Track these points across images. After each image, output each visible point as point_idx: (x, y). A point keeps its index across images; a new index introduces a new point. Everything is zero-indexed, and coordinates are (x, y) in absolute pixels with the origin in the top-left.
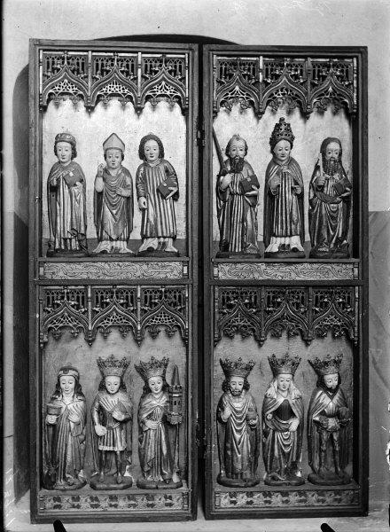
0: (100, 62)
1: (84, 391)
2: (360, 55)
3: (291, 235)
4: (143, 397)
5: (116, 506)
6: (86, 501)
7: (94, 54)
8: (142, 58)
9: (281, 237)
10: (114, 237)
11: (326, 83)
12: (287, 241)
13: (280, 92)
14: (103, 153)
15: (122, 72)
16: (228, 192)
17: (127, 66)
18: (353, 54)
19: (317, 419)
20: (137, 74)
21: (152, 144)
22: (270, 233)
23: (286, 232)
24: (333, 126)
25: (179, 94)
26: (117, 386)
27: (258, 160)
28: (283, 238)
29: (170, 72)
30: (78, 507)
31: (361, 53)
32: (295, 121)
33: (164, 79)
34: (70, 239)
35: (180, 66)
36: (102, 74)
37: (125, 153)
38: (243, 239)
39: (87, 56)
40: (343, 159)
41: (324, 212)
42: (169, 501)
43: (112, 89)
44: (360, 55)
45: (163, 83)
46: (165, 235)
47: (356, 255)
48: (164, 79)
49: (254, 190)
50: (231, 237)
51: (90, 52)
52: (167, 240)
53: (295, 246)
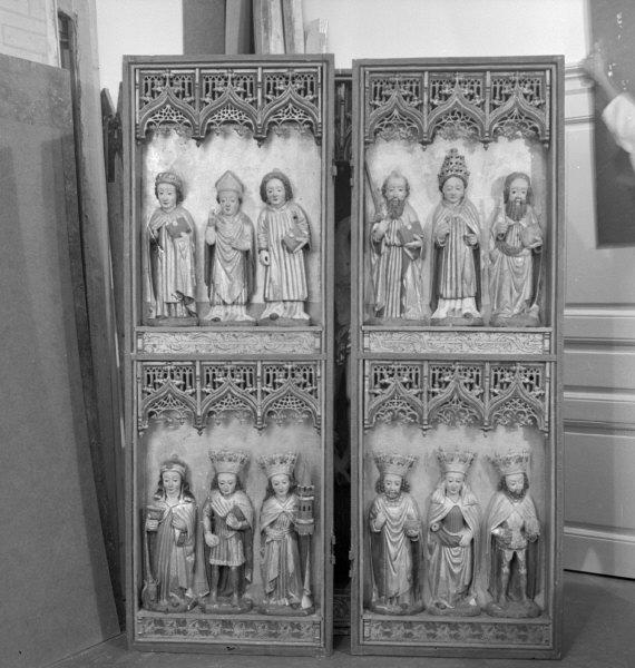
1: (194, 490)
4: (266, 499)
5: (230, 634)
6: (172, 625)
7: (496, 74)
8: (492, 77)
10: (229, 301)
11: (510, 103)
12: (457, 304)
13: (450, 117)
15: (239, 94)
19: (497, 532)
20: (422, 99)
21: (275, 184)
22: (436, 297)
25: (310, 119)
26: (234, 485)
27: (422, 207)
29: (299, 92)
30: (185, 633)
33: (290, 100)
34: (175, 304)
37: (469, 182)
42: (296, 630)
43: (226, 115)
44: (554, 67)
45: (290, 106)
46: (292, 298)
48: (290, 100)
49: (415, 240)
51: (260, 69)
52: (295, 304)
53: (469, 311)
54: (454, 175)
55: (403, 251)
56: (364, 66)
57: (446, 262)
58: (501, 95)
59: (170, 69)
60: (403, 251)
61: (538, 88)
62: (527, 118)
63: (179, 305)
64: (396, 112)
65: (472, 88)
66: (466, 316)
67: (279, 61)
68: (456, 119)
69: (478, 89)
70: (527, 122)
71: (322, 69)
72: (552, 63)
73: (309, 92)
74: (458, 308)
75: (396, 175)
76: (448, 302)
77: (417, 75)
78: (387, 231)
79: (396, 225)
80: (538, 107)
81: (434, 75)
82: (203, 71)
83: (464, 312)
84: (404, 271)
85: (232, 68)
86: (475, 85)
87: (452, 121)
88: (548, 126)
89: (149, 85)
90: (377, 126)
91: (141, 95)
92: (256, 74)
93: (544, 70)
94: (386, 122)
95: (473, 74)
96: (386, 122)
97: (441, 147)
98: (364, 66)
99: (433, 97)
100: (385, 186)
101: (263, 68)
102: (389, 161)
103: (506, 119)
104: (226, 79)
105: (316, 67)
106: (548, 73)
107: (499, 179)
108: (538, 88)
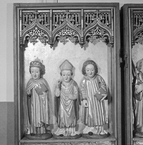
17: (74, 18)
20: (81, 23)
21: (90, 67)
33: (97, 25)
45: (97, 28)
48: (36, 26)
63: (42, 128)
85: (68, 10)
90: (137, 37)
92: (80, 13)
98: (130, 7)
99: (86, 22)
101: (53, 10)
104: (35, 15)
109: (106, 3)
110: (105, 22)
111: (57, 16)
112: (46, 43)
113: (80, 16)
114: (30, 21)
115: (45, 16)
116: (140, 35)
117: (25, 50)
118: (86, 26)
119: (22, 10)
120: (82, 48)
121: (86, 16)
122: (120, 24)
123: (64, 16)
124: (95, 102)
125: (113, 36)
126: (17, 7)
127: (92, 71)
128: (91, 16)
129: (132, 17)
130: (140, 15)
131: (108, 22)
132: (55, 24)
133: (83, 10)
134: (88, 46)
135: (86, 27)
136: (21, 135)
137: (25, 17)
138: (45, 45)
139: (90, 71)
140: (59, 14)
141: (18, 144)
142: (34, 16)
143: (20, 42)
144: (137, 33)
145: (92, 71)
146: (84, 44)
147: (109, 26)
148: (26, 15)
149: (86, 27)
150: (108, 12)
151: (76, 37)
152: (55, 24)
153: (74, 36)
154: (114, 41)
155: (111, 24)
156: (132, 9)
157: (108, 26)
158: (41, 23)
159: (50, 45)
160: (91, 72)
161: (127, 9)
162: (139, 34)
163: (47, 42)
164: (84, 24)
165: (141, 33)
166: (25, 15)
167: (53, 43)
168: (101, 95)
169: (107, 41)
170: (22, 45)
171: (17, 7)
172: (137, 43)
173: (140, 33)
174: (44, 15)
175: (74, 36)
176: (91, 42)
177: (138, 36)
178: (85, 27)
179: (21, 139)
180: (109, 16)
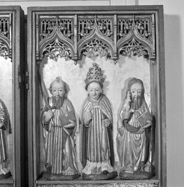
0: (45, 23)
2: (14, 13)
3: (101, 161)
9: (94, 162)
12: (98, 165)
13: (92, 43)
14: (85, 85)
16: (50, 125)
17: (66, 26)
18: (151, 12)
20: (73, 32)
22: (85, 159)
23: (97, 158)
24: (139, 68)
25: (5, 46)
27: (78, 98)
28: (95, 163)
31: (157, 10)
32: (106, 65)
35: (6, 24)
36: (47, 33)
38: (62, 163)
39: (73, 19)
40: (145, 95)
41: (129, 141)
47: (153, 175)
49: (70, 123)
50: (53, 160)
53: (106, 169)
54: (94, 81)
55: (63, 130)
56: (35, 11)
57: (90, 137)
58: (85, 30)
59: (97, 15)
60: (63, 130)
61: (147, 25)
62: (140, 44)
64: (57, 41)
65: (105, 25)
66: (106, 172)
67: (86, 11)
68: (95, 45)
69: (109, 26)
70: (140, 47)
71: (12, 15)
72: (155, 10)
73: (5, 30)
74: (98, 167)
75: (58, 80)
76: (92, 163)
77: (71, 17)
78: (53, 117)
79: (58, 113)
80: (147, 37)
81: (81, 17)
82: (41, 17)
83: (103, 170)
84: (63, 144)
86: (107, 24)
87: (93, 46)
88: (154, 49)
89: (45, 26)
90: (44, 50)
91: (39, 33)
92: (112, 19)
93: (151, 14)
94: (50, 47)
95: (106, 17)
96: (50, 47)
97: (88, 62)
98: (35, 11)
99: (81, 31)
100: (51, 87)
102: (56, 70)
103: (127, 45)
105: (36, 15)
106: (153, 16)
107: (126, 80)
108: (147, 25)
109: (3, 6)
110: (66, 33)
111: (45, 23)
112: (7, 57)
113: (113, 23)
114: (49, 30)
115: (68, 23)
116: (49, 47)
117: (44, 66)
118: (81, 37)
119: (39, 15)
120: (76, 64)
121: (109, 24)
122: (19, 33)
123: (53, 24)
124: (99, 128)
125: (11, 48)
126: (32, 11)
127: (96, 91)
128: (125, 23)
129: (37, 24)
130: (49, 21)
131: (148, 33)
132: (43, 33)
133: (116, 15)
134: (125, 62)
135: (80, 39)
136: (37, 175)
137: (43, 25)
138: (6, 58)
139: (94, 91)
140: (124, 20)
141: (33, 186)
142: (44, 23)
143: (36, 57)
144: (45, 44)
145: (59, 91)
146: (118, 59)
147: (111, 37)
148: (107, 22)
149: (80, 39)
150: (6, 18)
151: (146, 51)
152: (43, 33)
153: (143, 49)
154: (156, 56)
155: (113, 34)
156: (37, 13)
157: (109, 37)
158: (62, 31)
159: (113, 61)
160: (95, 92)
161: (31, 13)
162: (49, 46)
163: (8, 56)
164: (77, 34)
165: (51, 45)
166: (81, 22)
167: (79, 58)
168: (69, 119)
169: (146, 57)
170: (40, 60)
171: (32, 11)
172: (85, 56)
173: (49, 44)
174: (143, 22)
175: (143, 49)
176: (60, 56)
177: (47, 48)
178: (79, 39)
179: (37, 180)
180: (8, 22)
